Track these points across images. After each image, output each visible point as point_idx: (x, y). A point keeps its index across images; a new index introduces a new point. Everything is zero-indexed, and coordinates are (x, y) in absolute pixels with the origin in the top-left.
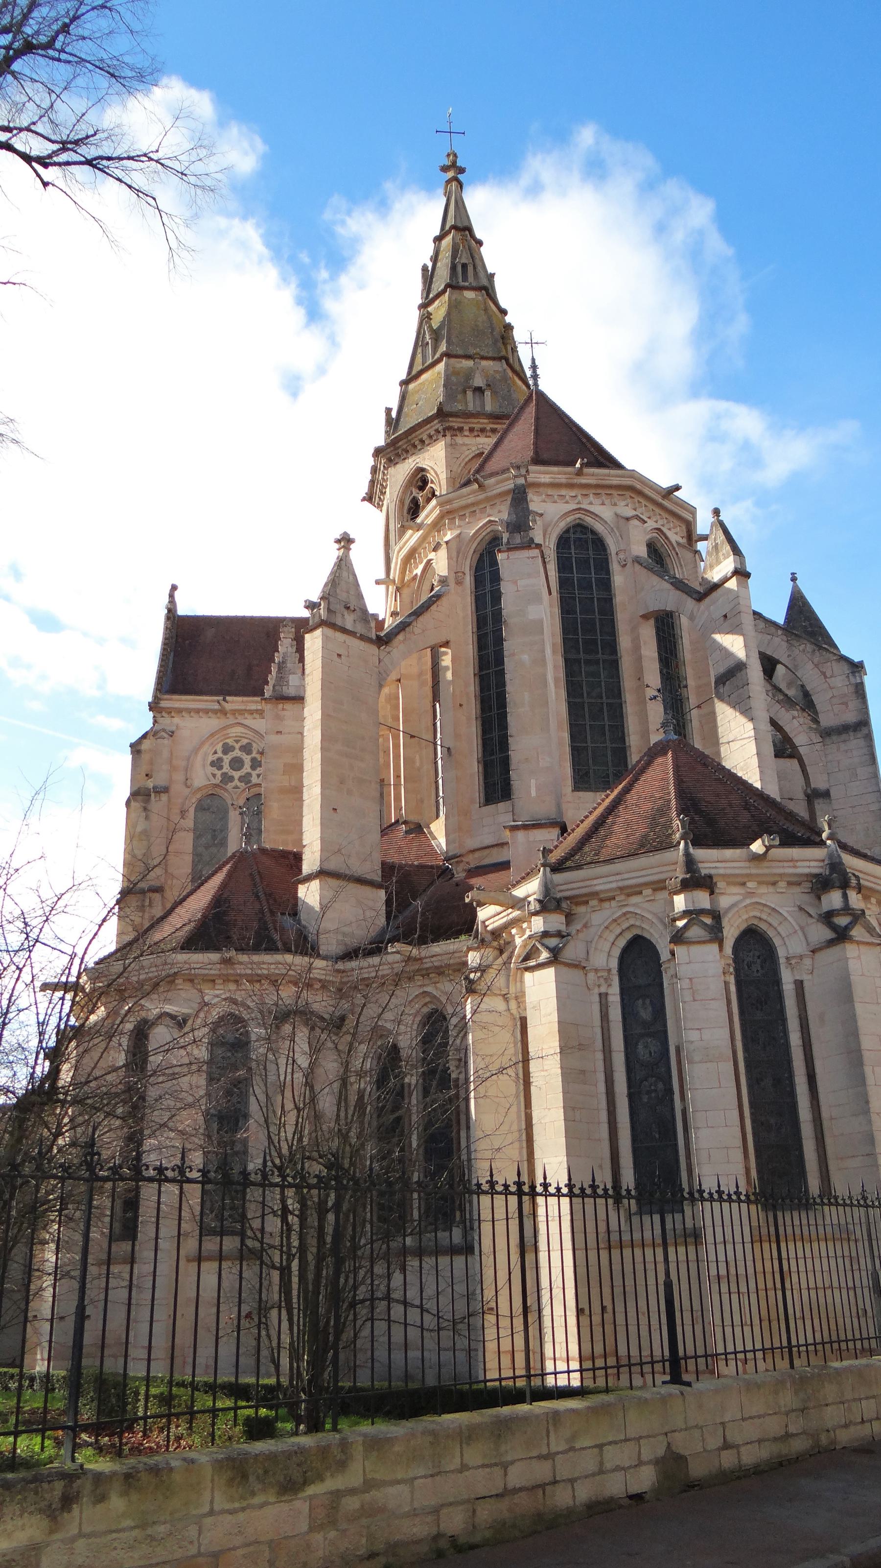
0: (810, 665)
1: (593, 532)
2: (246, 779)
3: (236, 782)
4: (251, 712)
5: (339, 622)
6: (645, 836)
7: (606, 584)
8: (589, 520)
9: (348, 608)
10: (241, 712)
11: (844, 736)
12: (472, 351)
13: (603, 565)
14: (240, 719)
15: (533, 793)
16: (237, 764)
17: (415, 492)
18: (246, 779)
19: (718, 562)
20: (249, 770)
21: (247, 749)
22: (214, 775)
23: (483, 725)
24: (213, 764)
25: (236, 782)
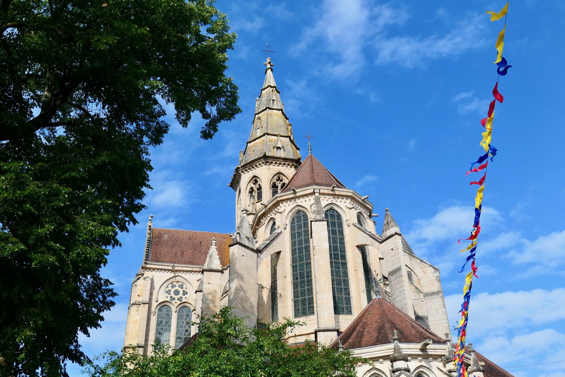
0: (419, 268)
1: (337, 212)
2: (180, 299)
3: (176, 300)
4: (184, 271)
5: (243, 243)
6: (377, 337)
7: (341, 233)
8: (335, 208)
9: (248, 239)
10: (180, 271)
11: (433, 297)
12: (276, 133)
13: (341, 225)
14: (180, 274)
15: (326, 317)
16: (177, 293)
17: (252, 185)
18: (180, 299)
19: (389, 229)
20: (182, 296)
21: (181, 286)
22: (167, 297)
23: (294, 285)
24: (167, 292)
25: (176, 300)
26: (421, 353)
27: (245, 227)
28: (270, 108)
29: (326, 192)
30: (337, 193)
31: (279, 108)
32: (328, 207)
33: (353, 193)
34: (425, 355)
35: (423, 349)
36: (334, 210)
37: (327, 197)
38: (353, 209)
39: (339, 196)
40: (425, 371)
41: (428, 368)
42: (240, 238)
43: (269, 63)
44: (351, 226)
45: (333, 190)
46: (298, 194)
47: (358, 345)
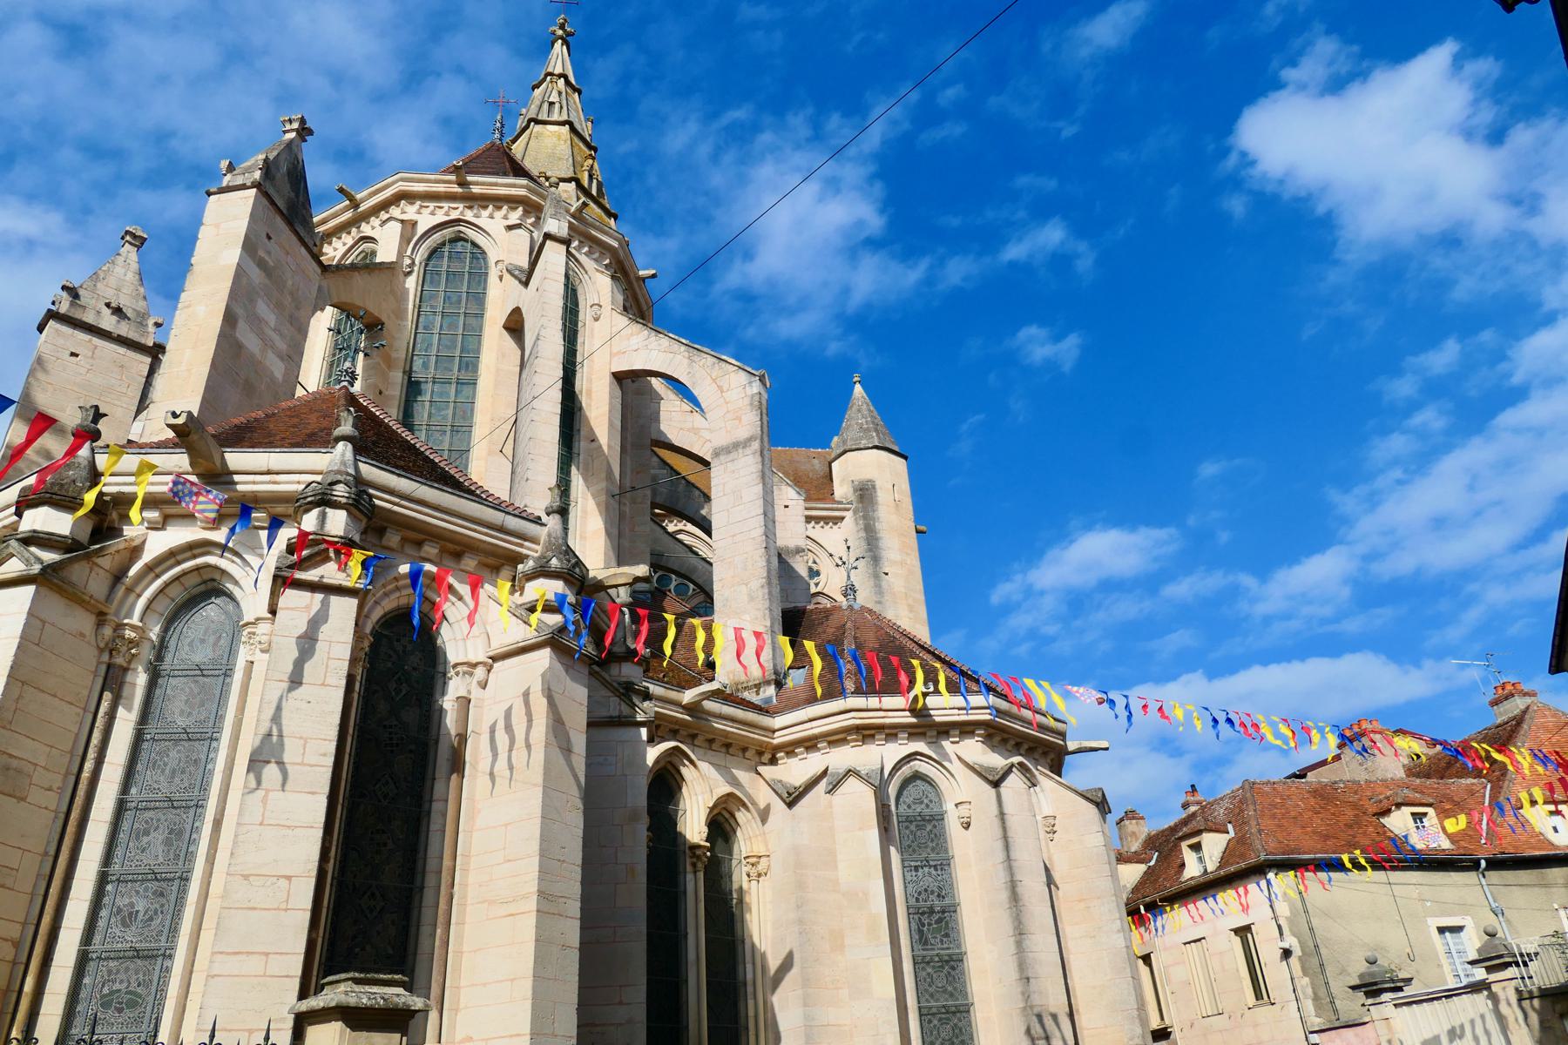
1: (474, 244)
8: (471, 233)
11: (732, 456)
26: (914, 720)
27: (112, 281)
29: (441, 188)
30: (476, 190)
31: (564, 117)
32: (448, 233)
33: (529, 189)
37: (446, 205)
39: (483, 201)
42: (72, 304)
43: (562, 27)
44: (507, 276)
45: (463, 184)
46: (363, 208)
47: (603, 641)
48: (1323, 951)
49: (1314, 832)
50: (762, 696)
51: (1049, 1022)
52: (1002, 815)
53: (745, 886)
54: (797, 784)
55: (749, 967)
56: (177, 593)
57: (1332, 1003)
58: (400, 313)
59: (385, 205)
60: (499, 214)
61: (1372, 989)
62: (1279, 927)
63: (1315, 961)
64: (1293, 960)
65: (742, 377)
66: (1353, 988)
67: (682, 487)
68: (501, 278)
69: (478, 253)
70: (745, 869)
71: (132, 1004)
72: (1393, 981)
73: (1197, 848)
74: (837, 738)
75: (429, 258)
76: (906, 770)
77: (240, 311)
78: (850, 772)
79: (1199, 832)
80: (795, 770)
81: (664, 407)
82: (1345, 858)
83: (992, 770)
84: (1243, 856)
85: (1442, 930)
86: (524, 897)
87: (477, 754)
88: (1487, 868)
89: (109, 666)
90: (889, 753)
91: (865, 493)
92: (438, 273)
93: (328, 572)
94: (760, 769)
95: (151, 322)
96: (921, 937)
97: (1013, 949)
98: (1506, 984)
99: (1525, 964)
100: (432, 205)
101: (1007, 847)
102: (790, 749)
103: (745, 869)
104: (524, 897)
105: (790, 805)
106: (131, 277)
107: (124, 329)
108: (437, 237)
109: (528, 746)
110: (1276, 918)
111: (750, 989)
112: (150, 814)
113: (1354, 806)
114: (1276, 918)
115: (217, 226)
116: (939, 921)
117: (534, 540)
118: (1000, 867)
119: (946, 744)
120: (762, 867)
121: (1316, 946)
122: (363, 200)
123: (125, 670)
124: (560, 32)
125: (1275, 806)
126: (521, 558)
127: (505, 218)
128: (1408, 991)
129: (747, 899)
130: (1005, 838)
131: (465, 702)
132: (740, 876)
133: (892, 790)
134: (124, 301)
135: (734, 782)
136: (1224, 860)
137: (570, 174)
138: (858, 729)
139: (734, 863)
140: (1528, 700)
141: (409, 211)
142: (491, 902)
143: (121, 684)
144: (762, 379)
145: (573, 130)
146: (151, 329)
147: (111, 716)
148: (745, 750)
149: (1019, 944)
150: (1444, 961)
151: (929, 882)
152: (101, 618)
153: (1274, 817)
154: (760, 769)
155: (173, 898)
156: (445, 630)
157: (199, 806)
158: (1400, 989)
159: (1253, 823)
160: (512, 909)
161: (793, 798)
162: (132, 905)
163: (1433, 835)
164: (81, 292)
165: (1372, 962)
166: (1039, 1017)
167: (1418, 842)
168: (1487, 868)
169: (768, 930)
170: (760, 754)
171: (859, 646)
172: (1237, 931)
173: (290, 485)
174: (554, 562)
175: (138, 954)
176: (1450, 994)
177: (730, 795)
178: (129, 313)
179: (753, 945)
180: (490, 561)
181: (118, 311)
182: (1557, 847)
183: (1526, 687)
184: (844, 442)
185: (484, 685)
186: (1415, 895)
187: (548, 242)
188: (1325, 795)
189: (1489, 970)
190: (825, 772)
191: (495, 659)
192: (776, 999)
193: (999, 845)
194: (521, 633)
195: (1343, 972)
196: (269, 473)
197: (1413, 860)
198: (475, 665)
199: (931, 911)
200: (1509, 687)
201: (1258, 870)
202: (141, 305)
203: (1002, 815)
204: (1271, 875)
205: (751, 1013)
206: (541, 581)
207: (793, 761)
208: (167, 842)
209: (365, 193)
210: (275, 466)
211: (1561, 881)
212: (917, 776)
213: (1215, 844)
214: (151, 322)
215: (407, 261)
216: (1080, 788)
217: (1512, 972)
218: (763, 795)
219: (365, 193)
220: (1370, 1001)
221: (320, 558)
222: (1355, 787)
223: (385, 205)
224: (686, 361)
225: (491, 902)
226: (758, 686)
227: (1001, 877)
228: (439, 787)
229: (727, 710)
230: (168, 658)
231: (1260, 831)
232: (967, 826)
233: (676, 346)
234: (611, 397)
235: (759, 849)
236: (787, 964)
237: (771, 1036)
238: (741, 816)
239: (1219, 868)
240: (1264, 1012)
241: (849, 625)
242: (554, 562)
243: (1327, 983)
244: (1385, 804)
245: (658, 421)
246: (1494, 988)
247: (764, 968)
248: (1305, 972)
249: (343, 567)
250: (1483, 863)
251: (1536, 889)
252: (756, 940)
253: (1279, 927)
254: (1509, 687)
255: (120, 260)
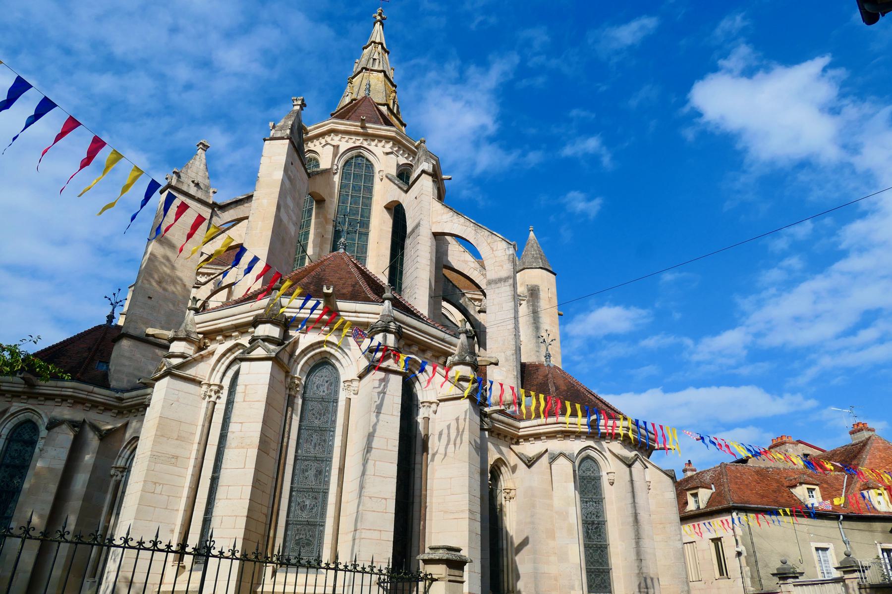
0: (485, 244)
1: (367, 160)
8: (366, 154)
11: (499, 285)
27: (194, 169)
28: (367, 69)
29: (352, 129)
30: (370, 131)
31: (381, 68)
32: (354, 152)
33: (397, 133)
34: (594, 434)
35: (593, 425)
36: (363, 157)
37: (354, 138)
38: (392, 156)
39: (373, 137)
40: (332, 351)
41: (340, 348)
42: (178, 181)
43: (380, 15)
44: (385, 180)
45: (363, 127)
48: (758, 555)
49: (757, 493)
50: (511, 409)
51: (649, 581)
52: (632, 481)
53: (503, 503)
54: (531, 456)
55: (505, 542)
56: (312, 363)
57: (760, 581)
58: (331, 195)
59: (322, 135)
60: (380, 145)
61: (783, 575)
62: (737, 541)
63: (753, 559)
64: (742, 558)
65: (504, 245)
66: (774, 575)
67: (450, 287)
68: (381, 180)
69: (370, 166)
70: (503, 495)
71: (308, 544)
72: (794, 573)
73: (695, 495)
74: (551, 435)
75: (344, 166)
76: (584, 454)
77: (282, 203)
78: (561, 454)
79: (697, 488)
80: (530, 449)
81: (450, 247)
82: (781, 511)
83: (627, 458)
84: (720, 503)
85: (817, 549)
86: (462, 511)
87: (433, 444)
88: (844, 520)
89: (289, 395)
90: (575, 446)
91: (534, 292)
92: (350, 174)
93: (390, 363)
94: (512, 446)
95: (211, 191)
96: (587, 535)
97: (634, 545)
98: (853, 580)
99: (864, 571)
100: (347, 137)
101: (634, 497)
102: (527, 438)
103: (503, 495)
104: (462, 511)
105: (529, 467)
106: (202, 167)
107: (199, 195)
108: (349, 154)
109: (455, 444)
110: (735, 536)
111: (505, 552)
112: (307, 463)
113: (777, 481)
114: (735, 536)
115: (270, 158)
116: (596, 528)
117: (455, 346)
118: (630, 506)
119: (604, 443)
120: (512, 493)
121: (754, 552)
122: (311, 131)
123: (295, 397)
124: (379, 18)
125: (736, 477)
126: (448, 354)
127: (383, 147)
128: (801, 579)
129: (504, 509)
130: (633, 492)
131: (427, 419)
132: (501, 498)
133: (577, 464)
134: (199, 179)
135: (501, 452)
136: (710, 502)
137: (384, 102)
138: (562, 432)
139: (498, 491)
140: (871, 433)
141: (335, 140)
142: (445, 512)
143: (294, 403)
144: (514, 248)
145: (386, 76)
146: (211, 194)
147: (291, 418)
148: (505, 437)
149: (638, 543)
150: (817, 565)
151: (591, 509)
152: (287, 373)
153: (736, 483)
154: (512, 446)
155: (320, 500)
156: (417, 385)
157: (329, 460)
158: (797, 577)
159: (726, 486)
160: (456, 516)
161: (530, 463)
162: (304, 502)
163: (816, 500)
164: (182, 175)
165: (784, 563)
166: (645, 579)
167: (809, 502)
168: (844, 520)
169: (514, 525)
170: (512, 439)
171: (557, 389)
172: (713, 540)
173: (373, 319)
174: (467, 358)
175: (308, 523)
176: (823, 582)
177: (500, 459)
178: (202, 185)
179: (507, 532)
180: (437, 354)
181: (197, 185)
182: (879, 512)
183: (869, 426)
184: (524, 263)
185: (435, 412)
186: (806, 530)
187: (423, 175)
188: (762, 474)
189: (845, 572)
190: (547, 451)
191: (441, 401)
192: (517, 558)
193: (630, 495)
194: (451, 390)
195: (766, 566)
196: (355, 312)
197: (805, 512)
198: (431, 403)
199: (593, 523)
200: (861, 426)
201: (728, 510)
202: (207, 182)
203: (632, 481)
204: (734, 514)
205: (505, 564)
206: (461, 367)
207: (527, 444)
208: (316, 476)
209: (312, 127)
210: (358, 310)
211: (879, 529)
212: (588, 457)
213: (704, 495)
214: (211, 191)
215: (335, 167)
216: (664, 469)
217: (857, 575)
218: (512, 459)
219: (312, 127)
220: (781, 582)
221: (385, 358)
222: (778, 471)
223: (322, 135)
224: (473, 232)
225: (445, 512)
226: (509, 405)
227: (629, 511)
228: (418, 458)
229: (501, 418)
230: (308, 391)
231: (729, 490)
232: (612, 484)
233: (468, 223)
234: (432, 245)
235: (510, 485)
236: (525, 542)
237: (515, 577)
238: (503, 469)
239: (707, 507)
240: (724, 582)
241: (550, 375)
242: (467, 358)
243: (758, 571)
244: (794, 482)
245: (447, 255)
246: (847, 581)
247: (512, 543)
248: (748, 565)
249: (397, 362)
250: (842, 517)
251: (867, 533)
252: (508, 529)
253: (737, 541)
254: (861, 426)
255: (198, 157)
